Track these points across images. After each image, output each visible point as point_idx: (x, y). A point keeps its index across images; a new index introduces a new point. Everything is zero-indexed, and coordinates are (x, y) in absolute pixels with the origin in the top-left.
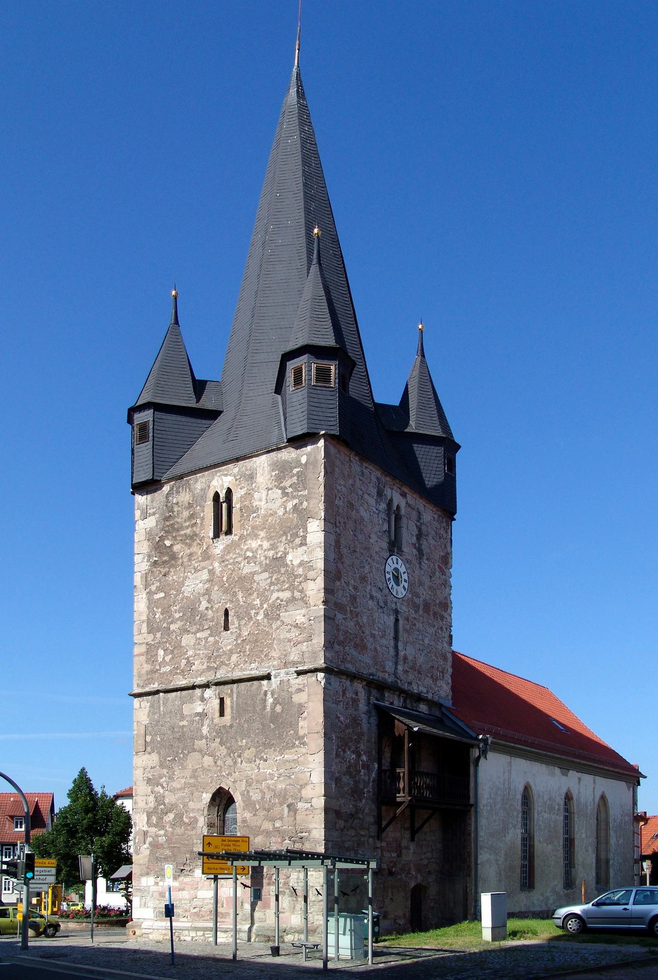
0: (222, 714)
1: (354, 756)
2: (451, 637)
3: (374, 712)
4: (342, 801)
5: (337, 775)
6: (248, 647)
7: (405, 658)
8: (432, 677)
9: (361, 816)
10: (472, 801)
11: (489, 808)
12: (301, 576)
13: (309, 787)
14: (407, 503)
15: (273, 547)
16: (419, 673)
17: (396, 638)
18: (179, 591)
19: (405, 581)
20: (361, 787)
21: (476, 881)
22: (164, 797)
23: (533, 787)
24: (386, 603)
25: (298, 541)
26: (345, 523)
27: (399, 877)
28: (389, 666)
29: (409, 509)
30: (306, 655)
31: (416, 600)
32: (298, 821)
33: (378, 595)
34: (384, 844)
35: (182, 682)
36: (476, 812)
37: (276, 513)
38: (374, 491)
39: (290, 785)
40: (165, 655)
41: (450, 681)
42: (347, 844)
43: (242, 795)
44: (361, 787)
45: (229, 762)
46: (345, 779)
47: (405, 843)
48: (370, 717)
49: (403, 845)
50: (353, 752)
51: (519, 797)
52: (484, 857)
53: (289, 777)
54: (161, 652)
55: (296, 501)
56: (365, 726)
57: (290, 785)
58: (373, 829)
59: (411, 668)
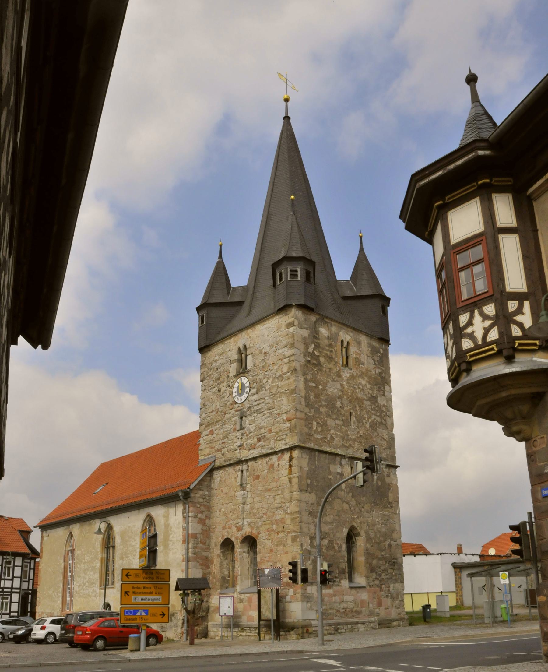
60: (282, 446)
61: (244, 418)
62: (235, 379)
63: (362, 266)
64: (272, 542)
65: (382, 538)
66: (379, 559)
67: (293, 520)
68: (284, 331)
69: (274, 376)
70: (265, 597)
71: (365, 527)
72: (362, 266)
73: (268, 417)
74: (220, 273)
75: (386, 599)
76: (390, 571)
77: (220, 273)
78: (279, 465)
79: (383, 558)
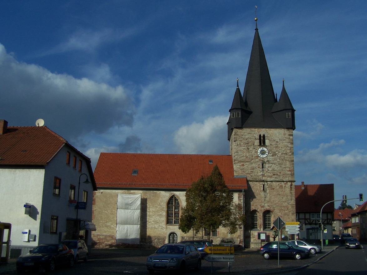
60: (287, 179)
61: (264, 164)
62: (259, 147)
64: (281, 214)
67: (292, 207)
68: (287, 136)
69: (282, 152)
70: (284, 233)
73: (279, 167)
78: (285, 186)
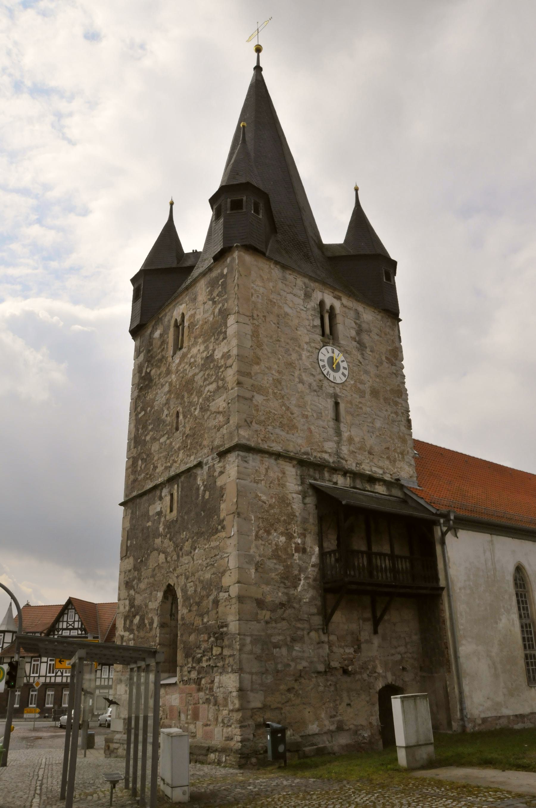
0: (171, 511)
1: (283, 539)
2: (409, 421)
3: (310, 492)
4: (267, 589)
5: (258, 558)
6: (189, 441)
7: (350, 440)
8: (388, 458)
9: (296, 606)
10: (442, 583)
11: (468, 591)
12: (222, 366)
13: (228, 574)
14: (342, 304)
15: (207, 348)
16: (370, 453)
17: (337, 418)
18: (152, 407)
19: (344, 368)
20: (296, 572)
21: (458, 678)
22: (134, 599)
23: (527, 566)
24: (321, 387)
25: (221, 337)
26: (264, 316)
27: (358, 677)
28: (330, 446)
29: (344, 309)
30: (226, 437)
31: (361, 387)
32: (220, 614)
33: (311, 380)
34: (333, 638)
35: (149, 485)
36: (449, 596)
37: (208, 320)
38: (301, 293)
39: (214, 574)
40: (142, 463)
41: (413, 462)
42: (275, 640)
43: (182, 590)
44: (296, 572)
45: (175, 557)
46: (270, 564)
47: (365, 635)
48: (304, 498)
49: (362, 639)
50: (282, 534)
51: (510, 578)
52: (466, 648)
53: (213, 565)
54: (140, 462)
55: (220, 305)
56: (297, 506)
57: (214, 574)
58: (317, 620)
59: (360, 449)
63: (359, 222)
65: (204, 593)
66: (198, 631)
71: (182, 580)
72: (359, 222)
74: (169, 236)
75: (206, 706)
76: (216, 651)
77: (169, 236)
79: (207, 629)
